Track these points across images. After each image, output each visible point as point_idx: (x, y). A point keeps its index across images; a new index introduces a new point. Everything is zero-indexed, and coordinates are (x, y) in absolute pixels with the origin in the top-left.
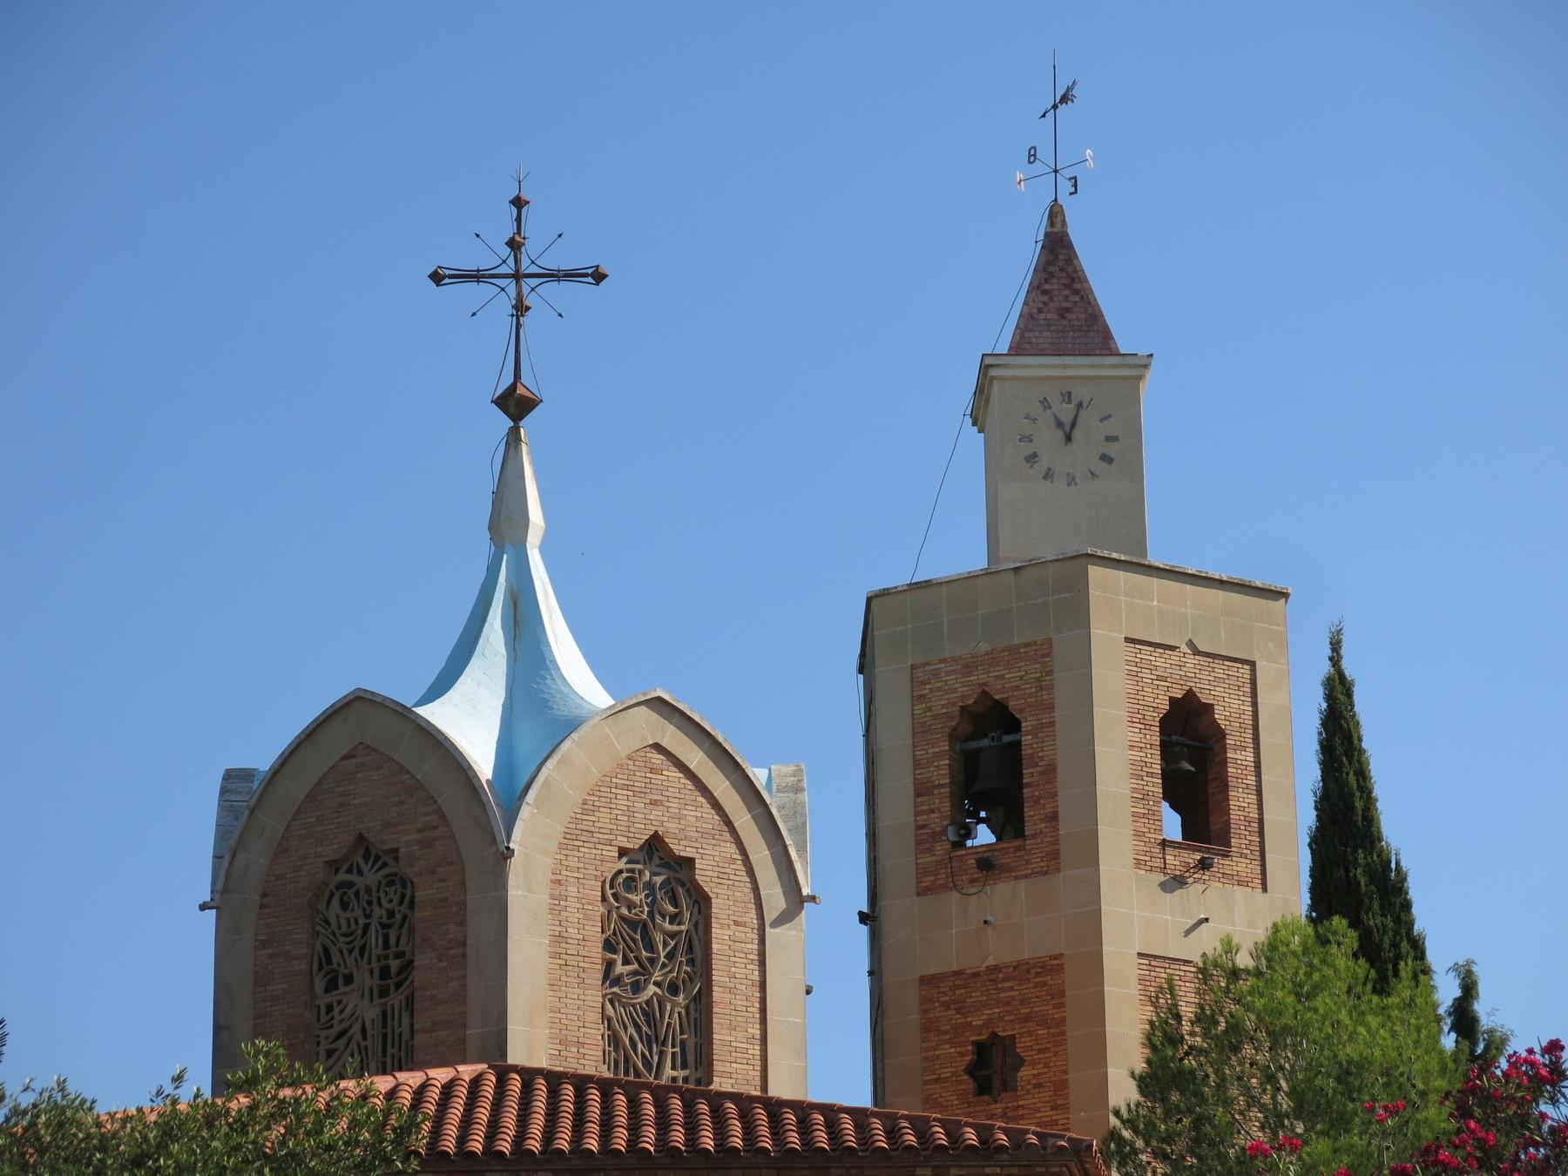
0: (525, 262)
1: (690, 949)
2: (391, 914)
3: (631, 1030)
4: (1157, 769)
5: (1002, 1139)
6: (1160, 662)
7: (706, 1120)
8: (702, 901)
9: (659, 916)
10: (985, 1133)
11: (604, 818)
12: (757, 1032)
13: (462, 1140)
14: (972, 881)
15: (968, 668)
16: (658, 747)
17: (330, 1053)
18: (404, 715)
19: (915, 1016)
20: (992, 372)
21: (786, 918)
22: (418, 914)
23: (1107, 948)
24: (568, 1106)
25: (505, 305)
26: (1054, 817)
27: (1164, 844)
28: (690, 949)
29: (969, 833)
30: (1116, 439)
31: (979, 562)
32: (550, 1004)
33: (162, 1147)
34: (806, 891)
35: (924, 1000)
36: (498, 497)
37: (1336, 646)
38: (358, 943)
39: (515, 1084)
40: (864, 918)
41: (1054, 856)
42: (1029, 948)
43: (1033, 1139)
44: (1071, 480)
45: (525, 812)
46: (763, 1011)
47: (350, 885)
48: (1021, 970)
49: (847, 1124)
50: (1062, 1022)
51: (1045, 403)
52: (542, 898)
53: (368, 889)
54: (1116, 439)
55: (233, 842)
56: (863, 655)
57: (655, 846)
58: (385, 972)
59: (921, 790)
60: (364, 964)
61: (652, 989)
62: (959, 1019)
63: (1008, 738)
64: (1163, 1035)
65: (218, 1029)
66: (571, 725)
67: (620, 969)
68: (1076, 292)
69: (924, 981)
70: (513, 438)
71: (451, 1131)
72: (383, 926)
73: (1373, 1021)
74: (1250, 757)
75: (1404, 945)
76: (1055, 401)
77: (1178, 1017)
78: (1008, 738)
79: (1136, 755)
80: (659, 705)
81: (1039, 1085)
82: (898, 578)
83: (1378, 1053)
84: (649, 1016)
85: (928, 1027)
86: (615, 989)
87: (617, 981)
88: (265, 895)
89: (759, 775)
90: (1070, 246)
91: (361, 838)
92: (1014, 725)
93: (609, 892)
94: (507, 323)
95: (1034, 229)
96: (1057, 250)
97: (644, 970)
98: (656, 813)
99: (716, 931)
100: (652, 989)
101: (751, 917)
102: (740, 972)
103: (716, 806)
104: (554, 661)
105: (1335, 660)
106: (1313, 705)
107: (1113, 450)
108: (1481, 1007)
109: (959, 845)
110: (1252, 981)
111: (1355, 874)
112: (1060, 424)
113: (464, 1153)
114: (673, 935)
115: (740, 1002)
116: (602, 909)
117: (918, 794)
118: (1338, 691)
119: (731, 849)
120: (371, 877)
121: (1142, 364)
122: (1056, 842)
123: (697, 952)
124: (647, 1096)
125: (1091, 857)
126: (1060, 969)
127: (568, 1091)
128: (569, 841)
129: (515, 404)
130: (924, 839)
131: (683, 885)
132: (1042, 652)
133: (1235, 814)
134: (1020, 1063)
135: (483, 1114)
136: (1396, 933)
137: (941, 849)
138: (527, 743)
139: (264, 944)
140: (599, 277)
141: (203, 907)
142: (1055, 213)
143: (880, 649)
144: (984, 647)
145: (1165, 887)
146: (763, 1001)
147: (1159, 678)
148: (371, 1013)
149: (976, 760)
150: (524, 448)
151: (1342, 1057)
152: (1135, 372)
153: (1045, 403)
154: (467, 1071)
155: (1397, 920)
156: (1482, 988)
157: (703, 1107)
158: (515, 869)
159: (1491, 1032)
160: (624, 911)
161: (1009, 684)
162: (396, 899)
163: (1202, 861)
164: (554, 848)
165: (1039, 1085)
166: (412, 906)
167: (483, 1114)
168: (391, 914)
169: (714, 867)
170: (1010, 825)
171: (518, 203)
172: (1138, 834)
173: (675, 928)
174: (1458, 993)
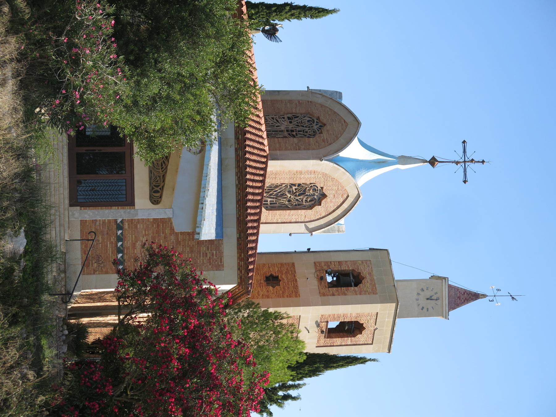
0: (461, 160)
1: (299, 205)
2: (306, 132)
3: (279, 191)
5: (250, 274)
7: (255, 204)
8: (311, 207)
9: (306, 197)
10: (252, 270)
11: (330, 183)
12: (279, 221)
13: (249, 146)
15: (370, 274)
16: (348, 196)
17: (273, 118)
18: (355, 134)
19: (285, 261)
20: (444, 280)
21: (307, 228)
22: (307, 139)
23: (302, 307)
24: (258, 172)
25: (457, 159)
26: (333, 295)
27: (327, 322)
28: (299, 205)
29: (329, 274)
30: (428, 310)
31: (396, 278)
32: (284, 171)
33: (239, 65)
34: (313, 233)
35: (288, 264)
36: (410, 158)
37: (374, 360)
38: (299, 124)
39: (264, 160)
40: (309, 249)
41: (324, 295)
42: (301, 289)
43: (250, 282)
44: (417, 300)
45: (332, 164)
46: (284, 223)
47: (314, 122)
48: (296, 287)
49: (254, 238)
50: (283, 297)
51: (436, 293)
52: (311, 169)
53: (312, 127)
54: (428, 310)
55: (324, 94)
56: (374, 249)
57: (324, 196)
58: (292, 131)
59: (340, 263)
60: (294, 126)
61: (289, 196)
62: (284, 272)
63: (353, 284)
64: (277, 316)
65: (278, 91)
66: (353, 176)
67: (294, 188)
68: (464, 301)
69: (293, 264)
71: (251, 143)
73: (281, 365)
74: (349, 343)
75: (300, 376)
77: (281, 319)
78: (353, 284)
79: (349, 315)
80: (358, 197)
81: (268, 291)
82: (392, 257)
83: (273, 366)
84: (282, 195)
85: (282, 265)
87: (291, 187)
88: (311, 102)
89: (342, 221)
91: (325, 125)
92: (356, 285)
94: (453, 160)
95: (480, 291)
96: (475, 296)
97: (294, 194)
98: (332, 196)
99: (303, 211)
100: (289, 196)
102: (294, 217)
103: (334, 211)
105: (370, 360)
106: (360, 355)
107: (425, 310)
108: (290, 401)
109: (327, 272)
110: (290, 337)
111: (316, 364)
112: (431, 297)
113: (246, 146)
114: (302, 200)
115: (286, 217)
116: (308, 183)
117: (339, 262)
118: (362, 360)
119: (323, 215)
120: (315, 127)
121: (447, 317)
122: (327, 295)
123: (298, 206)
124: (261, 191)
125: (323, 304)
126: (296, 297)
127: (262, 172)
128: (325, 175)
129: (433, 162)
130: (328, 264)
132: (374, 292)
133: (335, 339)
134: (274, 287)
135: (255, 151)
136: (304, 374)
137: (325, 268)
138: (349, 165)
139: (299, 102)
140: (465, 182)
141: (308, 87)
142: (484, 296)
143: (374, 252)
144: (375, 278)
145: (317, 322)
146: (286, 223)
148: (282, 128)
149: (347, 277)
150: (422, 164)
151: (272, 357)
153: (436, 293)
154: (267, 148)
155: (307, 374)
156: (294, 401)
157: (258, 204)
158: (317, 162)
159: (284, 404)
160: (308, 189)
161: (366, 284)
162: (310, 133)
163: (323, 331)
164: (323, 171)
165: (268, 291)
166: (308, 137)
167: (255, 151)
168: (306, 132)
169: (319, 210)
170: (332, 285)
171: (483, 162)
172: (330, 316)
174: (293, 396)
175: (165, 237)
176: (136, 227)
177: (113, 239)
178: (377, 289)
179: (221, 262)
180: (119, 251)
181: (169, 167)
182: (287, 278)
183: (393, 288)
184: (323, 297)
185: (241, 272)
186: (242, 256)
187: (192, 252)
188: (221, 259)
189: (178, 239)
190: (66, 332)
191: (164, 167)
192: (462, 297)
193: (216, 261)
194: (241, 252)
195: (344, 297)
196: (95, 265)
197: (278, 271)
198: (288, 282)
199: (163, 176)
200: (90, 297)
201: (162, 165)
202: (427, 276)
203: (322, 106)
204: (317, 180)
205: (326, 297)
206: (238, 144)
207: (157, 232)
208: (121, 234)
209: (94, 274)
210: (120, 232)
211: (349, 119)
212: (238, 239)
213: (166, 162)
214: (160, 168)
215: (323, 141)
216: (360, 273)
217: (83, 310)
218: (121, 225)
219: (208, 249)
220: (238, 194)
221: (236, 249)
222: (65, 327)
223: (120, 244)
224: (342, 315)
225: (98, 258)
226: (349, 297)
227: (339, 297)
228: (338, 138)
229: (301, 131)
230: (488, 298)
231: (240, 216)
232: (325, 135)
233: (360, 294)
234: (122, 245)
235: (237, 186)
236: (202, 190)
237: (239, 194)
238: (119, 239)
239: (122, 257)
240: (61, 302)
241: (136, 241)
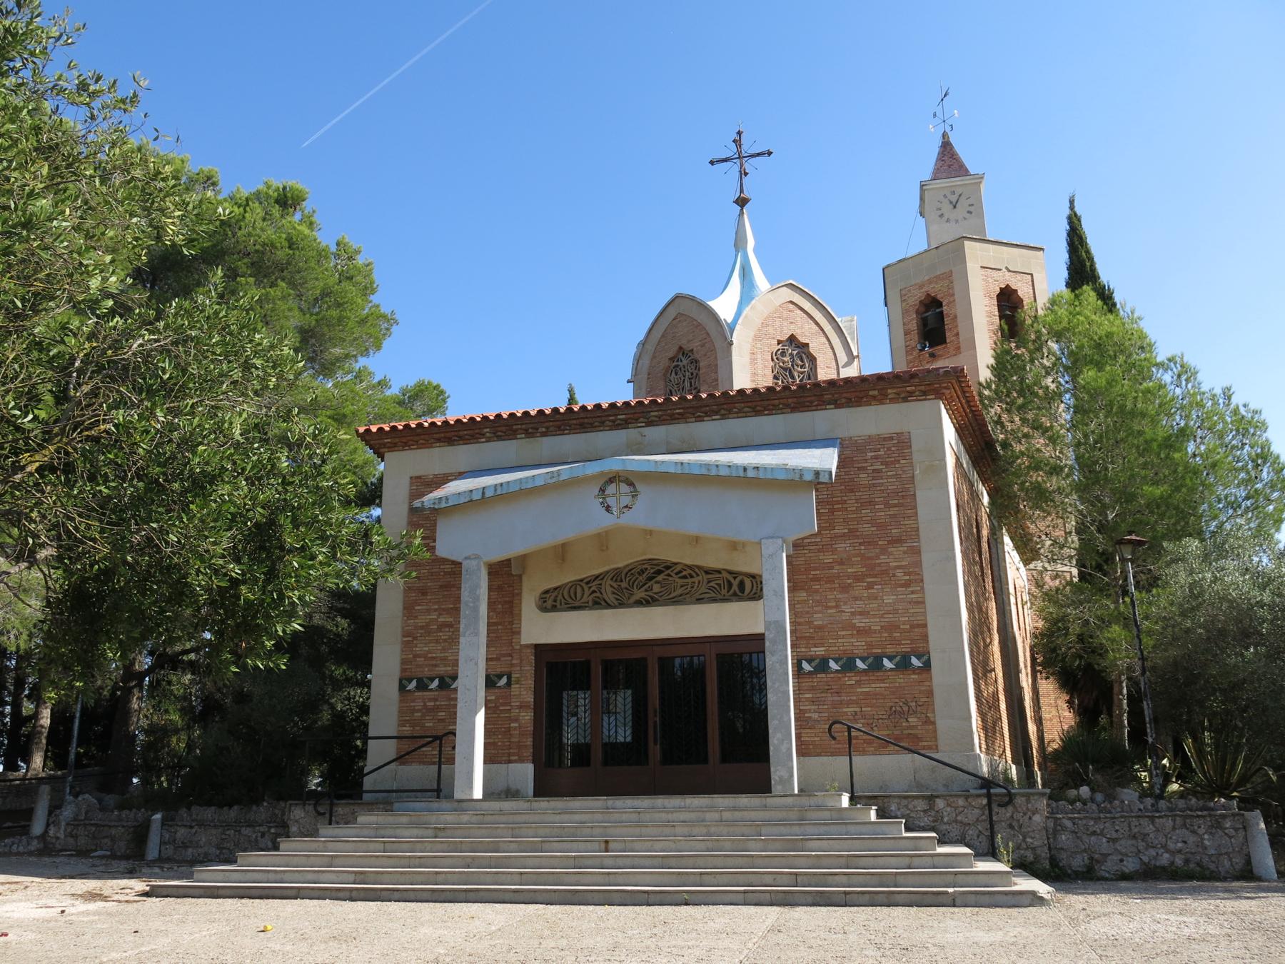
8: (813, 359)
11: (771, 329)
15: (921, 287)
37: (1072, 202)
41: (958, 348)
44: (957, 221)
51: (945, 196)
52: (747, 359)
57: (792, 339)
70: (741, 213)
80: (791, 286)
91: (681, 348)
92: (940, 304)
95: (938, 142)
96: (946, 146)
98: (792, 327)
103: (817, 324)
105: (1072, 208)
107: (971, 209)
119: (824, 339)
120: (685, 362)
128: (758, 337)
129: (742, 202)
132: (949, 275)
137: (915, 353)
153: (945, 196)
158: (735, 349)
161: (936, 290)
175: (841, 563)
176: (820, 628)
177: (850, 680)
179: (892, 439)
180: (876, 665)
181: (689, 562)
186: (876, 393)
187: (871, 503)
188: (885, 439)
189: (844, 535)
190: (1085, 790)
191: (689, 571)
192: (949, 161)
193: (889, 449)
194: (867, 396)
195: (959, 319)
196: (913, 720)
199: (707, 572)
200: (990, 729)
201: (685, 577)
203: (654, 357)
205: (962, 345)
206: (637, 421)
207: (830, 580)
208: (836, 661)
209: (934, 723)
210: (832, 665)
211: (672, 313)
212: (838, 406)
213: (678, 568)
214: (690, 580)
215: (703, 346)
217: (1015, 729)
218: (817, 661)
219: (864, 468)
220: (741, 414)
221: (859, 409)
222: (1072, 793)
223: (860, 664)
225: (896, 714)
226: (959, 310)
228: (700, 324)
231: (787, 406)
232: (695, 345)
234: (863, 660)
235: (723, 417)
236: (714, 472)
237: (740, 411)
238: (849, 666)
239: (890, 659)
240: (1010, 808)
241: (853, 627)
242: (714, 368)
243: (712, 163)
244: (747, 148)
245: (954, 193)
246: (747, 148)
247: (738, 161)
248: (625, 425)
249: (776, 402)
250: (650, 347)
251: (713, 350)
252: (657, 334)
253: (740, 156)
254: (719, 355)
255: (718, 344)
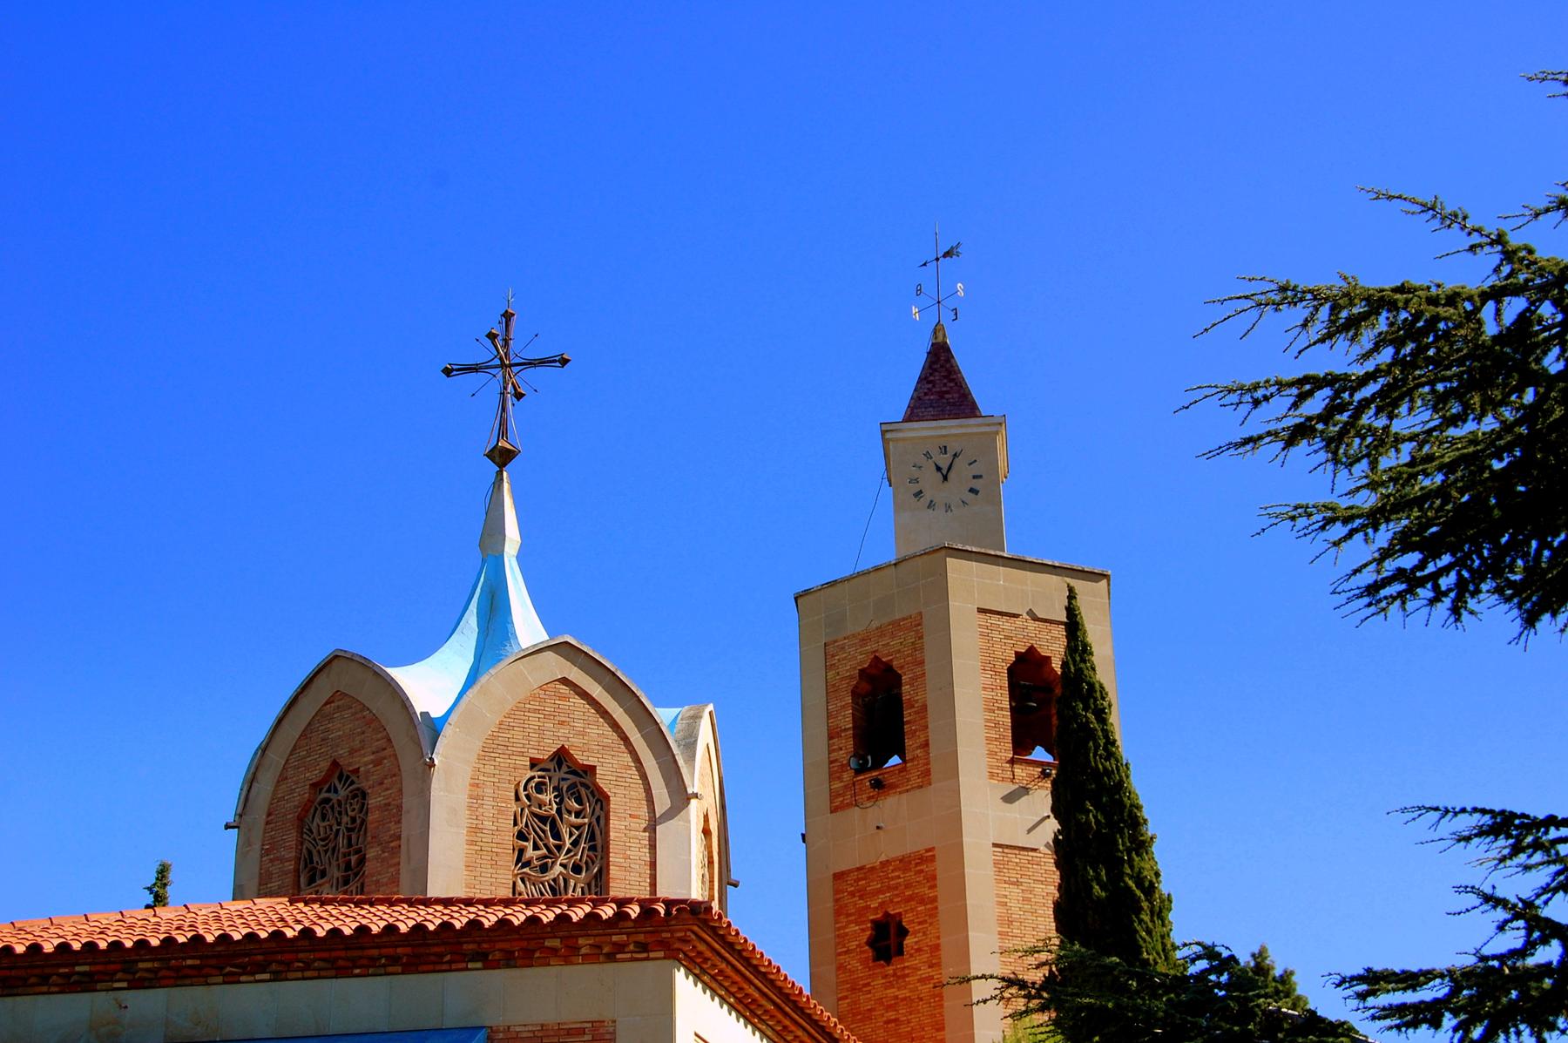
4: (1006, 705)
6: (1007, 626)
8: (602, 799)
11: (517, 735)
14: (869, 798)
15: (864, 641)
16: (565, 681)
19: (830, 904)
21: (671, 814)
22: (370, 818)
26: (926, 745)
28: (592, 837)
35: (837, 892)
38: (331, 845)
41: (927, 773)
42: (910, 847)
44: (948, 508)
48: (905, 862)
50: (934, 900)
51: (928, 455)
52: (462, 797)
53: (339, 802)
57: (561, 757)
58: (348, 866)
61: (558, 869)
62: (862, 903)
67: (530, 853)
68: (952, 380)
69: (839, 876)
70: (500, 473)
72: (349, 830)
76: (935, 453)
80: (564, 649)
81: (919, 950)
86: (526, 870)
87: (527, 864)
88: (269, 815)
90: (949, 350)
91: (335, 764)
92: (897, 679)
93: (522, 794)
96: (940, 360)
98: (563, 731)
101: (644, 811)
104: (514, 634)
107: (977, 484)
112: (939, 469)
114: (578, 827)
117: (830, 738)
119: (627, 758)
128: (488, 752)
129: (502, 457)
131: (587, 787)
132: (914, 624)
141: (227, 827)
144: (875, 624)
147: (1006, 637)
152: (993, 429)
153: (928, 455)
161: (892, 649)
164: (474, 758)
165: (919, 950)
168: (353, 820)
169: (612, 772)
172: (992, 754)
173: (579, 821)
178: (905, 615)
179: (582, 1031)
182: (880, 891)
183: (902, 567)
184: (934, 777)
185: (620, 948)
186: (556, 943)
192: (942, 388)
197: (857, 924)
198: (889, 888)
202: (888, 491)
203: (282, 778)
204: (506, 776)
205: (934, 767)
211: (323, 689)
215: (377, 763)
216: (862, 672)
220: (309, 971)
224: (989, 716)
226: (932, 698)
227: (933, 724)
229: (349, 838)
230: (946, 321)
231: (394, 960)
232: (364, 761)
233: (922, 663)
237: (308, 966)
242: (394, 811)
243: (447, 372)
244: (521, 348)
245: (944, 450)
246: (521, 348)
247: (499, 373)
248: (87, 984)
249: (375, 952)
250: (277, 758)
251: (396, 774)
252: (292, 732)
253: (505, 361)
254: (409, 785)
255: (407, 763)
